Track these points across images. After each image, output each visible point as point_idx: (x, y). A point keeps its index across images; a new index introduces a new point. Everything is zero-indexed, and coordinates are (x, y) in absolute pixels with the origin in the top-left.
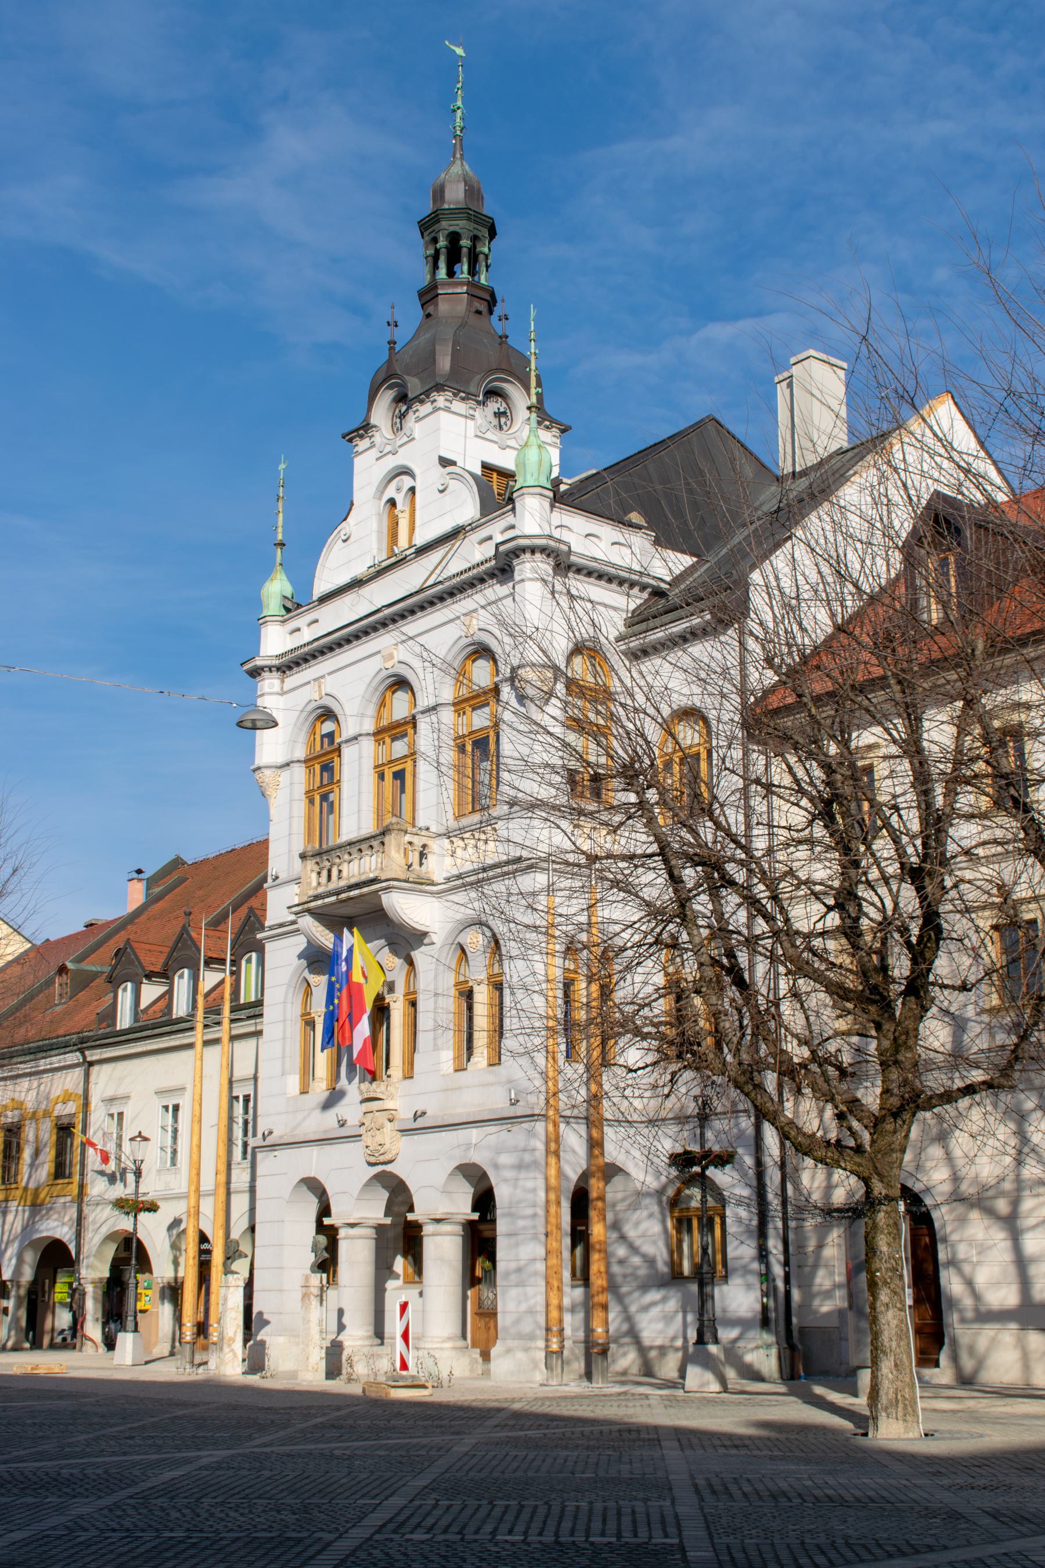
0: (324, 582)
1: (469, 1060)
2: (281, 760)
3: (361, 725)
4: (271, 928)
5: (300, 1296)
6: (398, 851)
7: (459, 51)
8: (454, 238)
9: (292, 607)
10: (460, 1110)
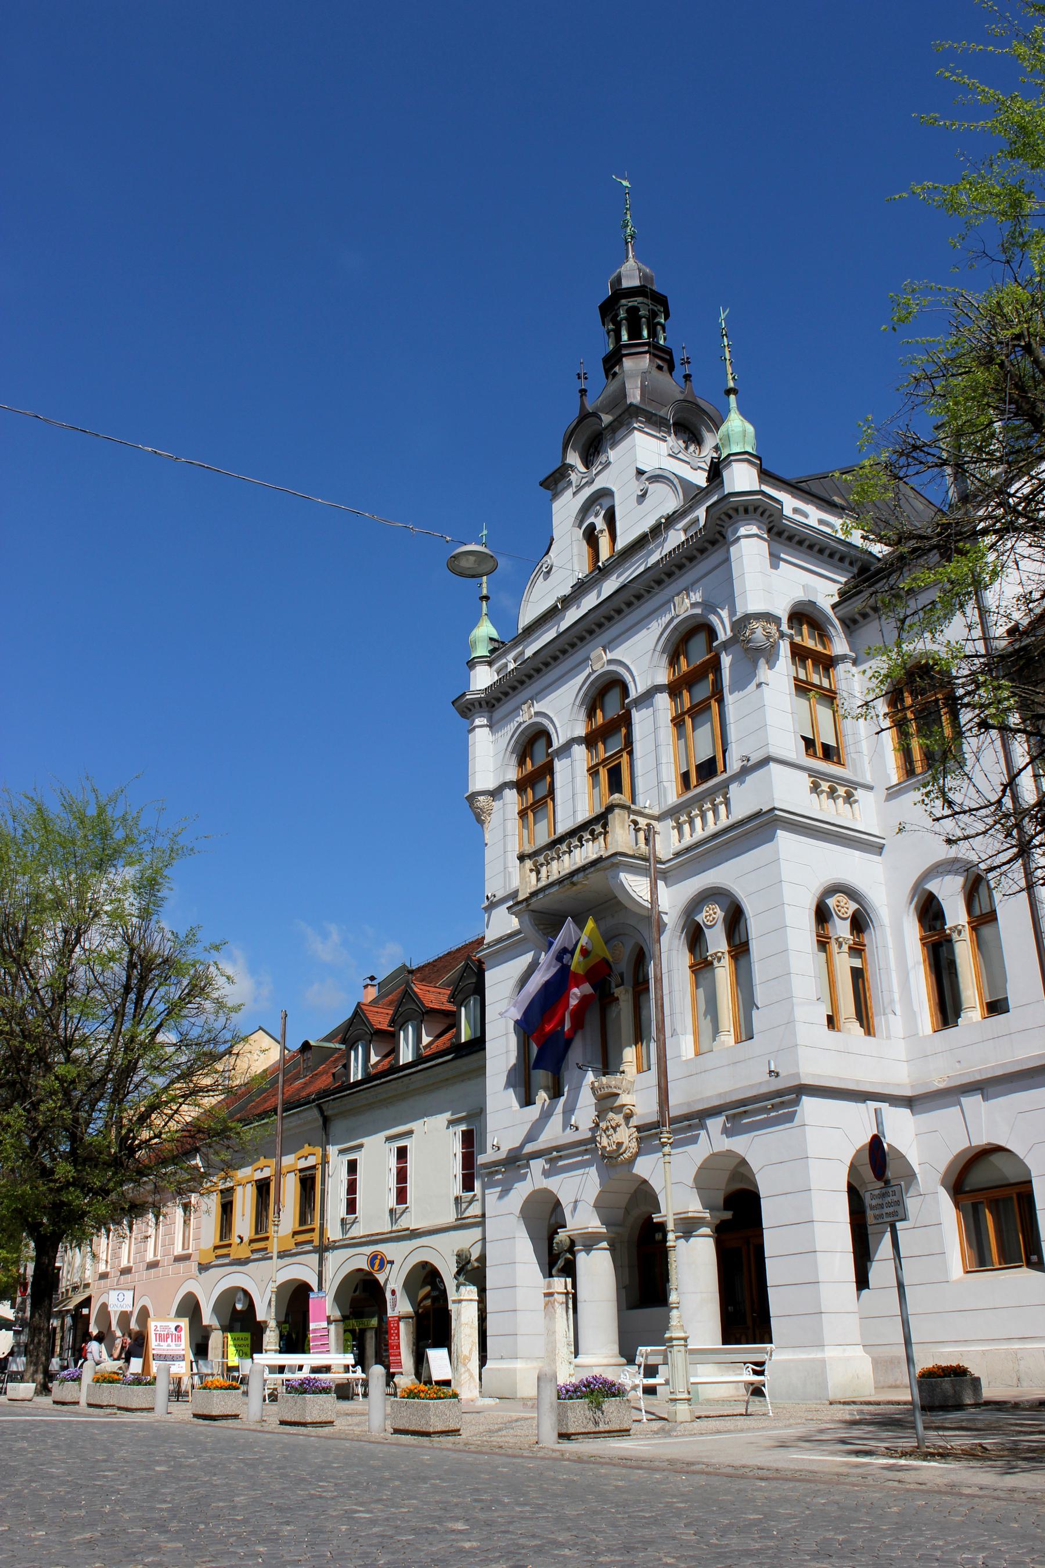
0: (528, 615)
1: (714, 1040)
2: (491, 786)
3: (572, 731)
4: (489, 946)
5: (543, 1305)
6: (623, 827)
7: (625, 183)
8: (633, 311)
9: (498, 648)
10: (709, 1093)
